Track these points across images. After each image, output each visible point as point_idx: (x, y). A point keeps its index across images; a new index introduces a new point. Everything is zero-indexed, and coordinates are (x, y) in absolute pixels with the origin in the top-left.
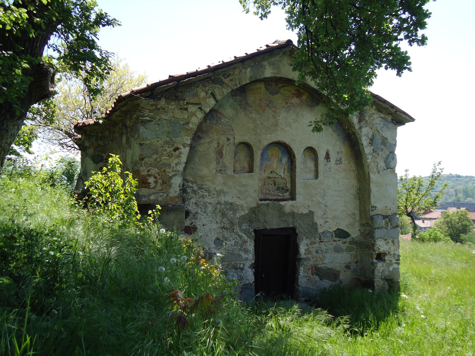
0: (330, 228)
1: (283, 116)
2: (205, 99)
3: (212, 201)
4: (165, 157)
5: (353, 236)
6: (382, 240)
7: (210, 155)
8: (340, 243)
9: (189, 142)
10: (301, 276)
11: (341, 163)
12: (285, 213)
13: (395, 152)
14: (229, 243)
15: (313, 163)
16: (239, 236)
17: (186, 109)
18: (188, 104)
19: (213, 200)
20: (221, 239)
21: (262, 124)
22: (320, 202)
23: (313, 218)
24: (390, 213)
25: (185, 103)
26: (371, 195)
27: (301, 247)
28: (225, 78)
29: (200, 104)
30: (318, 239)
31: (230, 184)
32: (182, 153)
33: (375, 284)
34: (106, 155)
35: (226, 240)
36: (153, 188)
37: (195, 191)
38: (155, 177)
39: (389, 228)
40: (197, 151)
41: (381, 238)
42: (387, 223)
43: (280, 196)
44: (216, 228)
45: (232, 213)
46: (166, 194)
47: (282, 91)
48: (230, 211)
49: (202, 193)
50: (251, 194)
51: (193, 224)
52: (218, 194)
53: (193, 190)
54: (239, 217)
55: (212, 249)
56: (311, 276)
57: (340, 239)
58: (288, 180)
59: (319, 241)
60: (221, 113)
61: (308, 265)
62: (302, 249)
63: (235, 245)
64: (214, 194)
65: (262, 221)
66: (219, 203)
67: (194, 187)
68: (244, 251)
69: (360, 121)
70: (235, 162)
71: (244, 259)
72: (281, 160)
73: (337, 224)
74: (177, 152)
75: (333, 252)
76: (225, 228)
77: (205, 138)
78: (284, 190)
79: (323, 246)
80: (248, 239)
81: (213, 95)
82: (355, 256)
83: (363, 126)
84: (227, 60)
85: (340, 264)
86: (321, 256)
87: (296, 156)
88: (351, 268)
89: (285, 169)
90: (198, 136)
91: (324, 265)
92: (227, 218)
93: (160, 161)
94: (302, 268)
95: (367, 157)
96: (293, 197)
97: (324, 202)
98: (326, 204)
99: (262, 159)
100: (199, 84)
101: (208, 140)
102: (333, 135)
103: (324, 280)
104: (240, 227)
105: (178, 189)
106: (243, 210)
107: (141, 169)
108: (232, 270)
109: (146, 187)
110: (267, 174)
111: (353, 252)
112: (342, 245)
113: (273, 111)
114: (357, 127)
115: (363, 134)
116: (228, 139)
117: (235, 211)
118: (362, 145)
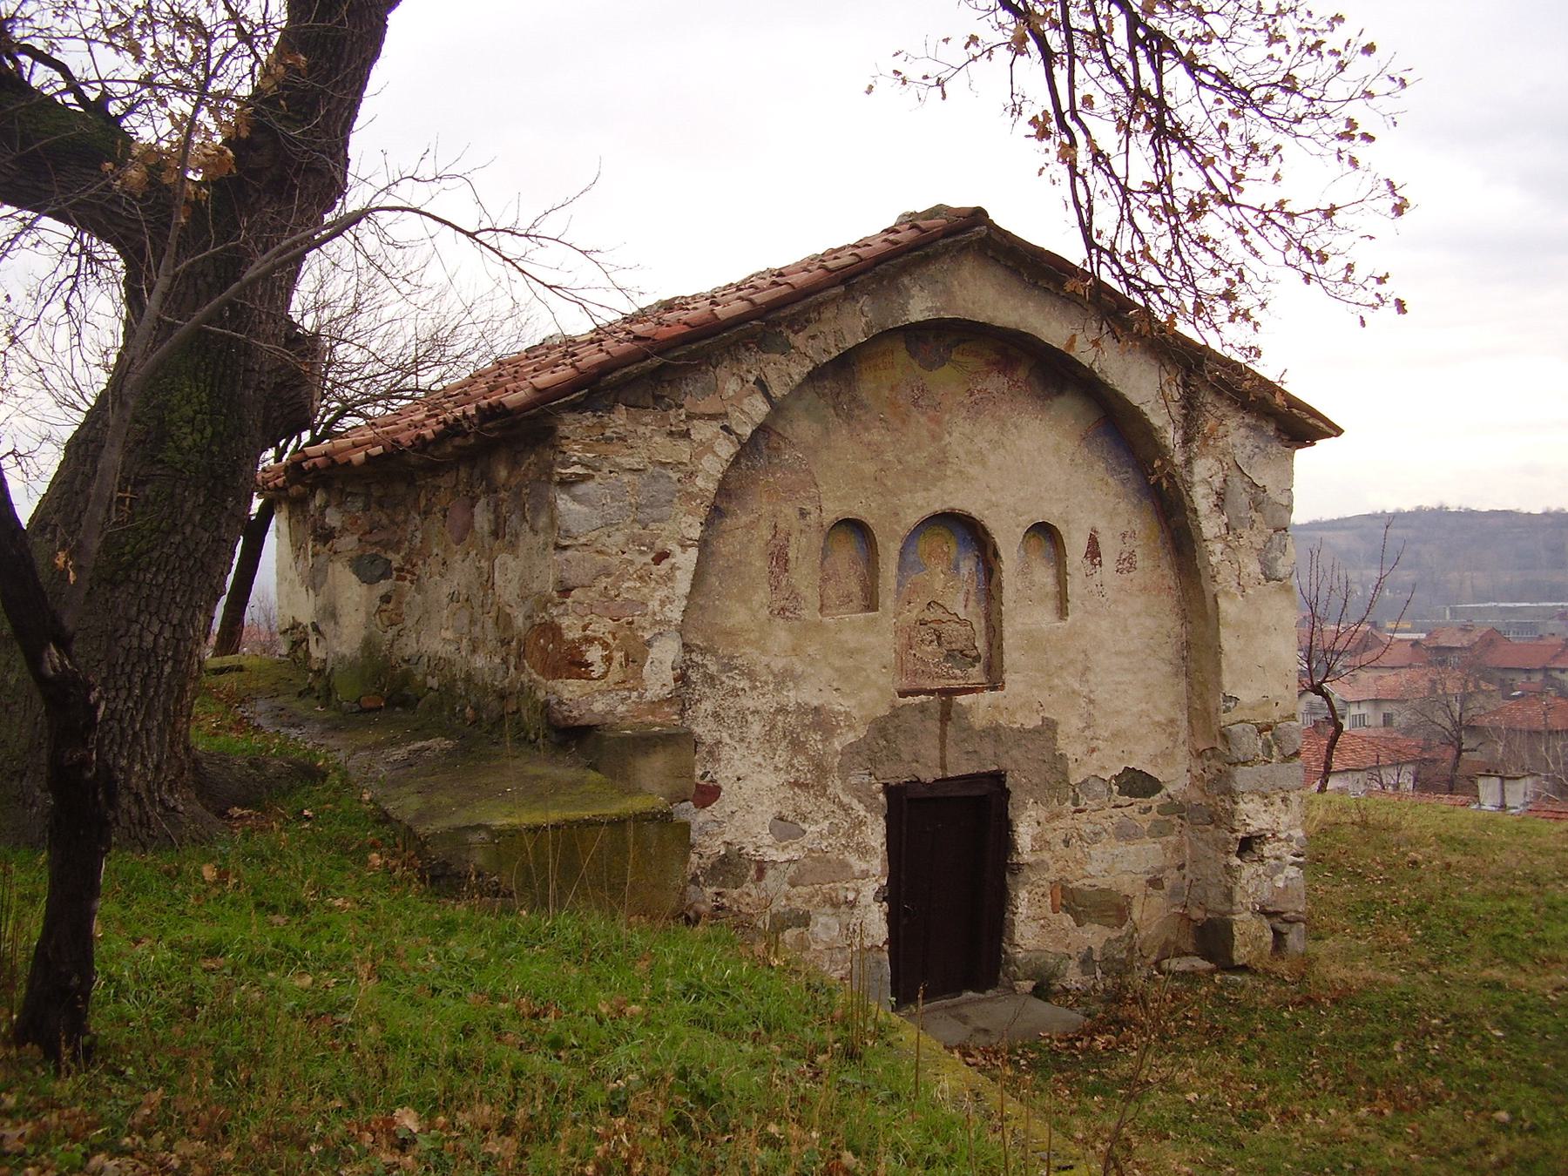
0: (1103, 768)
1: (960, 434)
2: (740, 401)
5: (1170, 789)
6: (1256, 798)
7: (750, 564)
9: (696, 533)
11: (1133, 567)
12: (971, 728)
15: (1052, 571)
16: (841, 805)
17: (686, 435)
21: (900, 462)
22: (1074, 692)
24: (1276, 714)
25: (683, 417)
26: (1224, 665)
27: (1020, 829)
28: (796, 333)
30: (1068, 804)
31: (811, 650)
32: (679, 568)
33: (1235, 928)
34: (398, 557)
36: (599, 679)
37: (712, 678)
38: (606, 646)
40: (713, 553)
42: (1270, 747)
44: (774, 786)
45: (819, 738)
46: (635, 693)
48: (815, 732)
49: (732, 683)
50: (873, 676)
51: (708, 778)
53: (705, 674)
54: (839, 749)
57: (1133, 800)
58: (979, 625)
61: (1041, 882)
62: (1025, 835)
63: (831, 833)
64: (766, 683)
65: (906, 757)
66: (782, 710)
67: (709, 664)
69: (1187, 441)
70: (823, 580)
72: (957, 567)
74: (665, 565)
75: (1113, 841)
77: (734, 514)
79: (1084, 824)
81: (761, 385)
82: (1177, 850)
87: (1002, 553)
88: (1166, 884)
94: (1023, 894)
95: (1211, 548)
96: (995, 683)
97: (1085, 690)
99: (901, 568)
101: (744, 519)
104: (844, 780)
105: (669, 676)
106: (851, 727)
107: (565, 622)
108: (824, 910)
109: (580, 677)
110: (913, 614)
111: (1170, 838)
112: (1138, 817)
113: (931, 419)
114: (1179, 459)
115: (1196, 478)
116: (803, 514)
118: (1195, 511)
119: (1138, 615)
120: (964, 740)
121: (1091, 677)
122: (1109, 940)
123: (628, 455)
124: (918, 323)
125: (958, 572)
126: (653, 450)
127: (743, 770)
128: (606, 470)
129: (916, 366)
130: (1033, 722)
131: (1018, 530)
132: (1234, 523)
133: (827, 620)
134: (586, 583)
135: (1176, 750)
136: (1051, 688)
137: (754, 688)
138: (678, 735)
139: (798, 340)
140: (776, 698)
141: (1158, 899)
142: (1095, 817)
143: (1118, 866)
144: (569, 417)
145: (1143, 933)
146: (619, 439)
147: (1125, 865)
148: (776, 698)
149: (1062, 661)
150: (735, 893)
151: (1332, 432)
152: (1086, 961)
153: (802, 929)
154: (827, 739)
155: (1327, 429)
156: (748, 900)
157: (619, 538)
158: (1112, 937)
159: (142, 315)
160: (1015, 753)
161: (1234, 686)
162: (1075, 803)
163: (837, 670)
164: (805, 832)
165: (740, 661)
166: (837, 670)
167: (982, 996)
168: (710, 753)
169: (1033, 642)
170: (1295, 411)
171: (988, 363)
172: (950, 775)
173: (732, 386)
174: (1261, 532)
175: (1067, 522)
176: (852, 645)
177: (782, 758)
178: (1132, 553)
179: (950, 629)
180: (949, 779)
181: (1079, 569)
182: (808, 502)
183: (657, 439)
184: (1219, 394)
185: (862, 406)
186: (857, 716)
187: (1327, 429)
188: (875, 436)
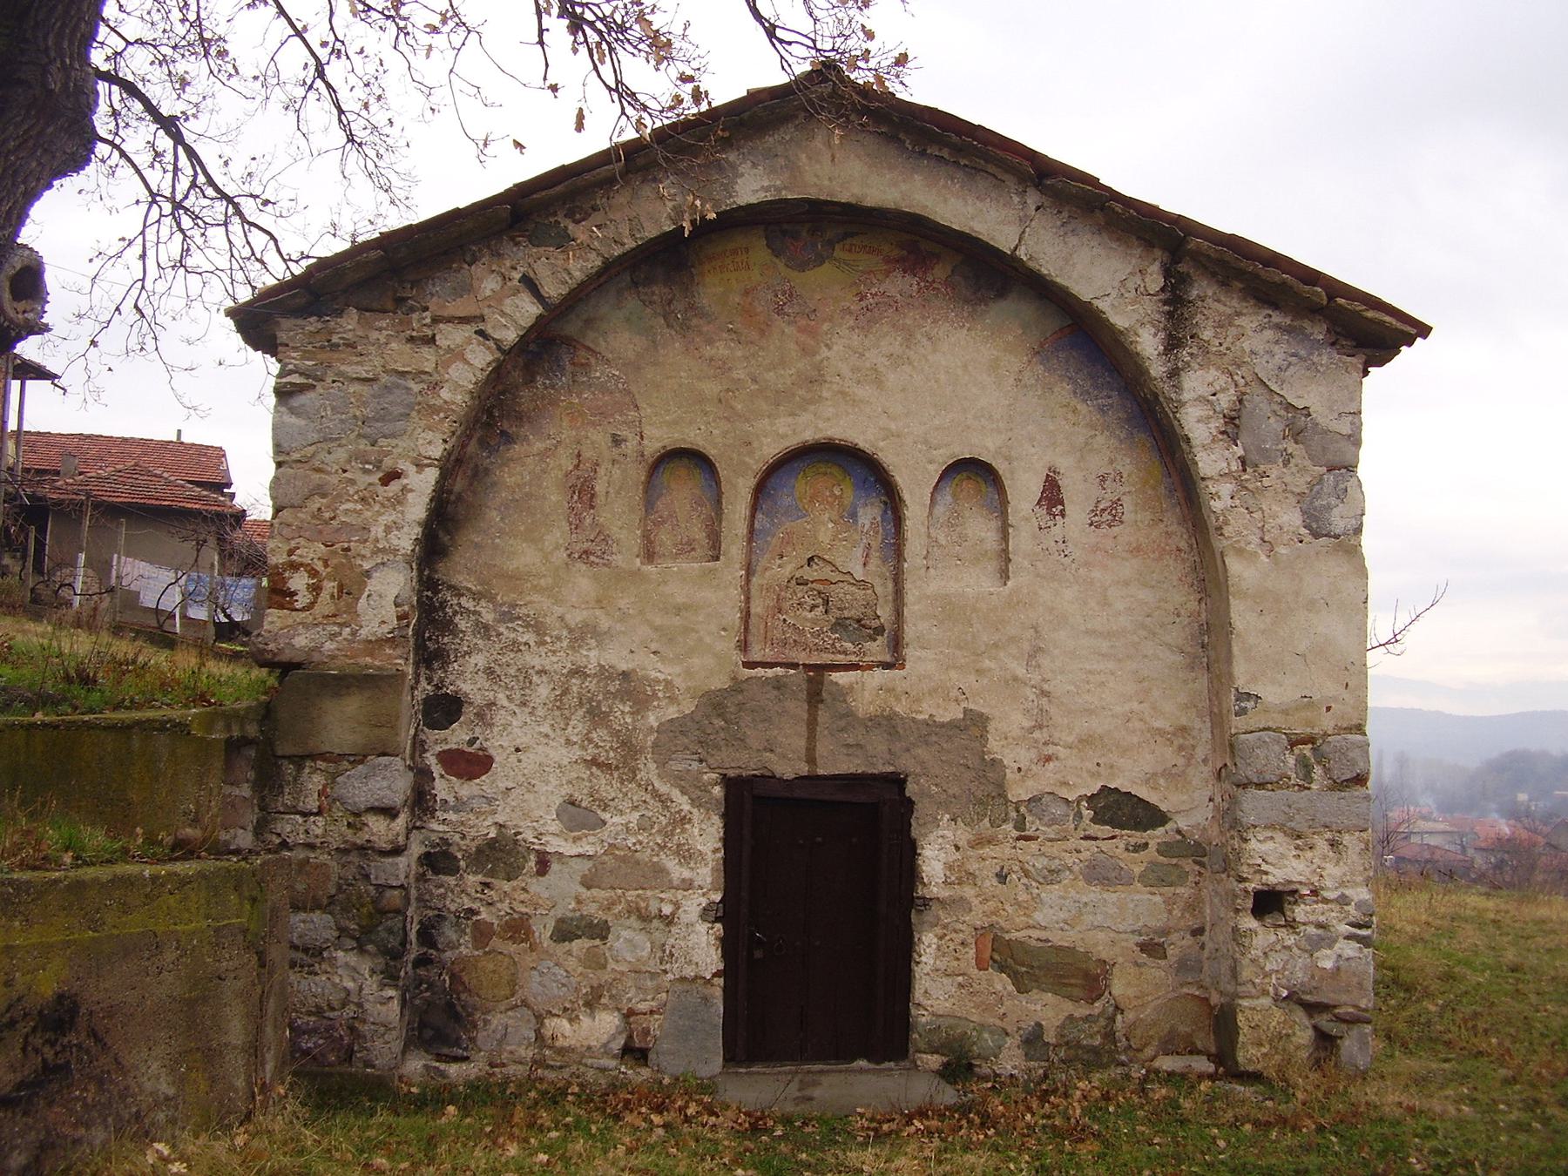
0: (1066, 784)
2: (500, 301)
3: (549, 662)
4: (350, 506)
5: (1182, 823)
6: (1279, 836)
8: (1117, 848)
10: (927, 969)
12: (850, 714)
13: (1362, 471)
14: (616, 819)
15: (995, 524)
16: (656, 795)
17: (432, 340)
18: (436, 320)
19: (554, 659)
20: (583, 804)
21: (754, 380)
22: (1016, 679)
23: (983, 738)
24: (1327, 723)
25: (428, 321)
26: (1235, 650)
28: (577, 222)
30: (1009, 827)
31: (622, 603)
32: (411, 491)
33: (1240, 1017)
35: (604, 810)
36: (303, 609)
37: (486, 627)
38: (313, 573)
39: (1314, 786)
41: (1271, 827)
43: (845, 653)
44: (565, 762)
45: (627, 709)
47: (838, 253)
49: (512, 635)
50: (708, 640)
51: (477, 745)
53: (477, 623)
54: (655, 725)
55: (548, 838)
56: (974, 972)
57: (1117, 832)
58: (884, 589)
59: (1015, 834)
60: (589, 349)
61: (960, 926)
62: (934, 861)
63: (641, 828)
64: (559, 638)
65: (754, 743)
66: (578, 672)
68: (677, 853)
69: (1172, 344)
71: (676, 883)
73: (1101, 769)
74: (395, 486)
75: (1081, 883)
76: (599, 765)
78: (864, 628)
80: (695, 811)
81: (530, 284)
85: (1112, 935)
86: (1023, 896)
87: (906, 496)
88: (1170, 952)
90: (503, 433)
91: (1035, 934)
92: (609, 727)
93: (331, 519)
96: (895, 662)
98: (1046, 687)
99: (755, 508)
100: (480, 250)
101: (539, 446)
102: (1075, 411)
103: (1035, 995)
104: (662, 765)
105: (390, 613)
106: (672, 699)
108: (628, 923)
109: (282, 607)
111: (1180, 890)
113: (801, 330)
114: (1157, 369)
115: (1186, 396)
116: (617, 441)
118: (1188, 440)
120: (842, 730)
122: (1071, 1017)
123: (357, 363)
124: (750, 206)
125: (856, 522)
126: (387, 358)
127: (524, 739)
128: (329, 380)
130: (953, 713)
131: (931, 467)
132: (1254, 457)
133: (650, 568)
135: (1191, 771)
138: (381, 678)
139: (579, 232)
140: (571, 658)
141: (1157, 972)
142: (1054, 849)
143: (1088, 919)
144: (286, 323)
145: (1130, 1016)
146: (348, 345)
147: (1100, 918)
148: (571, 658)
149: (996, 637)
150: (507, 886)
151: (1413, 331)
152: (1033, 1041)
153: (597, 942)
154: (638, 712)
155: (1399, 325)
156: (524, 896)
157: (341, 454)
158: (1077, 1015)
159: (1004, 502)
160: (920, 752)
161: (1253, 679)
162: (1020, 824)
163: (656, 629)
164: (604, 823)
166: (656, 629)
167: (872, 1066)
168: (480, 715)
169: (950, 610)
170: (1341, 301)
171: (887, 261)
172: (821, 772)
173: (490, 285)
175: (1009, 459)
176: (680, 600)
177: (577, 727)
178: (1117, 503)
179: (839, 592)
180: (819, 777)
181: (1027, 519)
182: (624, 427)
183: (394, 345)
184: (1224, 284)
185: (702, 314)
186: (683, 686)
187: (1399, 325)
188: (721, 350)
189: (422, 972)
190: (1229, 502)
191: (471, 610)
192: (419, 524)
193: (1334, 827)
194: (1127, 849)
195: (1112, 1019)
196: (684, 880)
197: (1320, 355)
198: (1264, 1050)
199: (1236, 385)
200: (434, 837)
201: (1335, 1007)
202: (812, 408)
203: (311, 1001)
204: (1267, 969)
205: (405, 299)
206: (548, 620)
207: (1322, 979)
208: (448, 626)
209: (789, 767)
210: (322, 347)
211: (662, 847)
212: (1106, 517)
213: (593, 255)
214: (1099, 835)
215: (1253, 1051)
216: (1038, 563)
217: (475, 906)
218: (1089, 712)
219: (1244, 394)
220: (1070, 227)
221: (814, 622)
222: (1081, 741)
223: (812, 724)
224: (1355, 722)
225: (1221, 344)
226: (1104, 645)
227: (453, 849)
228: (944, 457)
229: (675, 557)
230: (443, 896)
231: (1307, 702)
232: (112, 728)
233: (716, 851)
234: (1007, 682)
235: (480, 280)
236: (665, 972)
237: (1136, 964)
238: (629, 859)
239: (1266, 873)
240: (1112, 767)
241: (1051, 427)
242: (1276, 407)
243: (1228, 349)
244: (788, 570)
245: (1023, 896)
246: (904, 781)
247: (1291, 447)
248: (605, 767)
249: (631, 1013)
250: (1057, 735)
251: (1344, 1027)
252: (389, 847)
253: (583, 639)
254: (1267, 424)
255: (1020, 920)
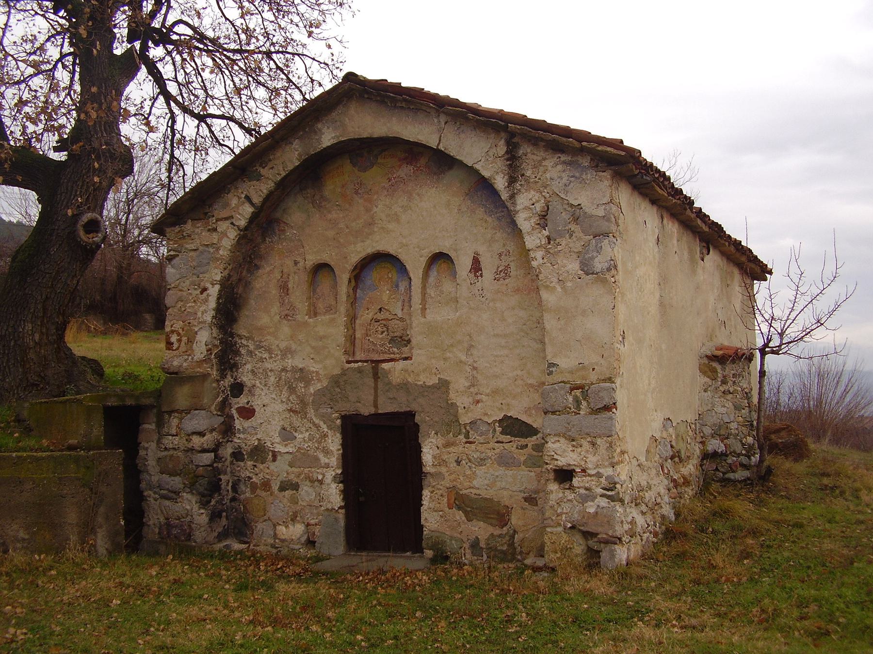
0: (486, 414)
1: (382, 206)
2: (238, 209)
4: (190, 304)
6: (562, 440)
11: (507, 275)
12: (390, 383)
16: (315, 425)
17: (215, 230)
21: (347, 227)
22: (461, 362)
23: (447, 392)
24: (593, 377)
28: (264, 168)
29: (232, 217)
30: (462, 437)
31: (300, 337)
37: (251, 352)
38: (179, 334)
47: (379, 161)
50: (332, 351)
52: (282, 355)
54: (313, 392)
57: (513, 439)
59: (464, 440)
60: (285, 223)
61: (439, 487)
62: (428, 456)
64: (277, 355)
66: (284, 370)
68: (323, 451)
69: (512, 181)
72: (397, 286)
73: (504, 407)
74: (205, 294)
76: (293, 411)
79: (473, 451)
80: (329, 431)
81: (248, 198)
83: (519, 190)
84: (462, 100)
85: (510, 493)
86: (468, 472)
89: (404, 301)
91: (474, 491)
92: (296, 394)
98: (475, 365)
101: (268, 269)
102: (486, 221)
103: (475, 522)
104: (316, 410)
105: (204, 349)
106: (319, 380)
115: (518, 208)
117: (308, 383)
119: (513, 309)
120: (388, 391)
121: (475, 352)
125: (398, 289)
127: (267, 401)
129: (356, 171)
130: (433, 381)
132: (553, 236)
134: (173, 305)
136: (445, 359)
137: (271, 358)
139: (263, 171)
142: (481, 448)
143: (498, 484)
146: (188, 236)
153: (295, 492)
156: (268, 471)
157: (188, 282)
160: (421, 400)
162: (467, 436)
165: (265, 343)
166: (313, 348)
170: (584, 144)
172: (380, 412)
173: (234, 202)
174: (579, 239)
176: (321, 333)
177: (285, 394)
178: (508, 267)
180: (380, 414)
184: (535, 145)
186: (323, 374)
188: (334, 215)
189: (233, 504)
190: (541, 261)
191: (246, 345)
192: (214, 310)
193: (592, 435)
194: (517, 448)
195: (513, 537)
196: (326, 464)
197: (586, 174)
198: (558, 555)
199: (545, 198)
200: (236, 445)
201: (598, 534)
202: (370, 237)
203: (176, 514)
204: (559, 512)
205: (207, 213)
206: (273, 347)
207: (588, 517)
208: (237, 353)
209: (366, 410)
210: (180, 238)
211: (318, 448)
212: (502, 274)
213: (270, 182)
214: (504, 440)
215: (552, 555)
216: (471, 302)
217: (251, 475)
218: (496, 377)
219: (549, 202)
220: (461, 129)
221: (382, 339)
222: (493, 392)
223: (376, 389)
224: (608, 376)
225: (536, 177)
226: (503, 342)
227: (242, 450)
228: (427, 253)
229: (325, 314)
230: (239, 471)
231: (582, 366)
232: (61, 402)
233: (339, 450)
234: (457, 363)
235: (231, 200)
236: (321, 506)
237: (522, 508)
238: (306, 454)
239: (557, 460)
240: (508, 405)
241: (475, 232)
242: (566, 207)
243: (539, 179)
244: (370, 316)
245: (468, 472)
246: (415, 415)
247: (573, 227)
248: (295, 412)
249: (308, 525)
250: (481, 389)
251: (602, 545)
252: (200, 449)
253: (286, 354)
254: (560, 216)
255: (466, 484)
